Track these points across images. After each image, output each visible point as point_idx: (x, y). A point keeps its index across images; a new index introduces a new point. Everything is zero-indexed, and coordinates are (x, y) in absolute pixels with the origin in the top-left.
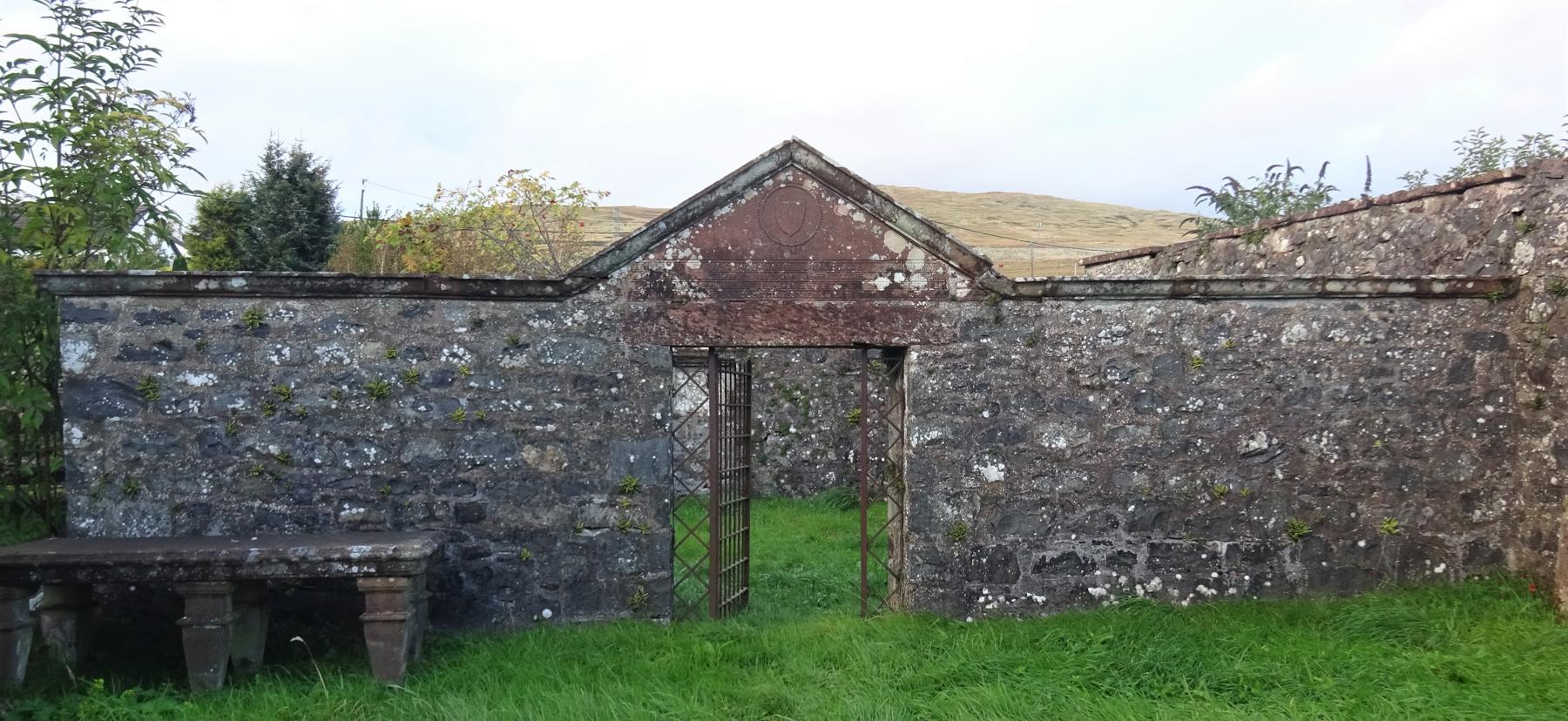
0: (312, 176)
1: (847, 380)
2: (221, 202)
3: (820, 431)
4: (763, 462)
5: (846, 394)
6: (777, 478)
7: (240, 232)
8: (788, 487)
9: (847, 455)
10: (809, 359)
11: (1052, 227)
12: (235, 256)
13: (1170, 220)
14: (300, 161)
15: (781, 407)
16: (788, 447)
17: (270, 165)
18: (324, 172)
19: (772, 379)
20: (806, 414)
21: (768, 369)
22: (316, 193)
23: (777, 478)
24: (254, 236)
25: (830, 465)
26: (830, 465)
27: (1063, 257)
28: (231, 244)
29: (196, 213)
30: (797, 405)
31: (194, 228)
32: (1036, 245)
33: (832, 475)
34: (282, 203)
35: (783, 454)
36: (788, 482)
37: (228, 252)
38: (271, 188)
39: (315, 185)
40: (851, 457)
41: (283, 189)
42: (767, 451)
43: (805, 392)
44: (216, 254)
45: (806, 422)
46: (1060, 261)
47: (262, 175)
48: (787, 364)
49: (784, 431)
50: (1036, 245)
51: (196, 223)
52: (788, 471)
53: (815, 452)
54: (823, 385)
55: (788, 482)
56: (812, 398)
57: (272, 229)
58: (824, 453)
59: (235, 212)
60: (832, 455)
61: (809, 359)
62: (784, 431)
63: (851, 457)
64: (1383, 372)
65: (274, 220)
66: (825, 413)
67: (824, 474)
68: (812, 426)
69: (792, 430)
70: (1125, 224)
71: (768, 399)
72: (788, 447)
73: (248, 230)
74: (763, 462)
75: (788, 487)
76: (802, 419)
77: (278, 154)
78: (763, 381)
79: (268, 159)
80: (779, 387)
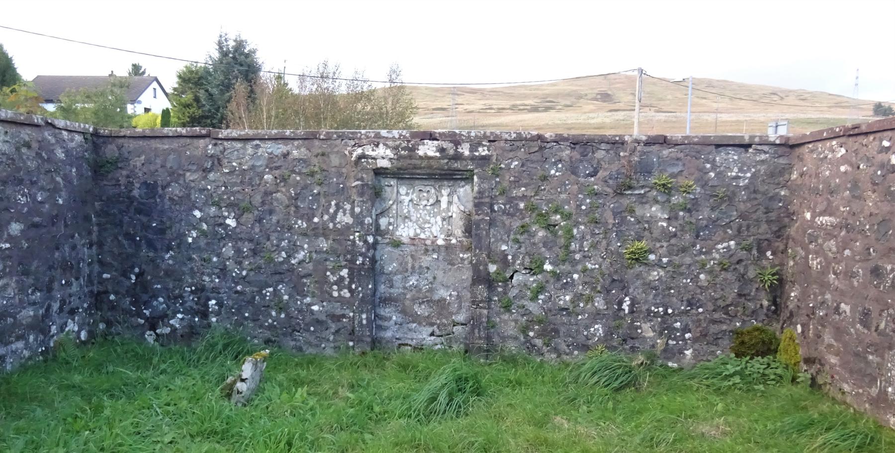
0: (247, 56)
1: (625, 202)
2: (191, 72)
3: (585, 270)
4: (507, 308)
5: (623, 220)
6: (525, 330)
7: (202, 91)
8: (539, 342)
9: (620, 303)
10: (574, 171)
11: (727, 100)
12: (199, 108)
13: (806, 96)
14: (240, 44)
15: (533, 235)
16: (541, 289)
17: (221, 48)
18: (254, 52)
19: (524, 197)
20: (567, 247)
21: (517, 183)
22: (249, 66)
23: (525, 330)
24: (211, 95)
25: (597, 316)
26: (597, 316)
27: (734, 119)
28: (197, 99)
29: (177, 80)
30: (555, 234)
31: (175, 89)
32: (717, 111)
33: (598, 329)
34: (227, 73)
35: (534, 298)
36: (539, 335)
37: (195, 104)
38: (222, 63)
39: (249, 60)
40: (626, 307)
41: (228, 63)
42: (512, 293)
43: (567, 216)
44: (187, 106)
45: (567, 257)
46: (733, 122)
47: (216, 55)
48: (545, 178)
49: (535, 268)
50: (717, 111)
51: (176, 86)
52: (540, 322)
53: (578, 297)
54: (592, 208)
55: (539, 335)
56: (577, 224)
57: (221, 90)
58: (590, 299)
59: (200, 79)
60: (599, 303)
61: (574, 171)
62: (535, 268)
63: (626, 307)
64: (855, 185)
65: (223, 84)
66: (594, 246)
67: (587, 327)
68: (574, 263)
69: (548, 267)
70: (776, 98)
71: (517, 224)
72: (541, 289)
73: (207, 91)
74: (507, 308)
75: (539, 342)
76: (562, 253)
77: (226, 40)
78: (511, 200)
79: (220, 44)
80: (532, 208)
